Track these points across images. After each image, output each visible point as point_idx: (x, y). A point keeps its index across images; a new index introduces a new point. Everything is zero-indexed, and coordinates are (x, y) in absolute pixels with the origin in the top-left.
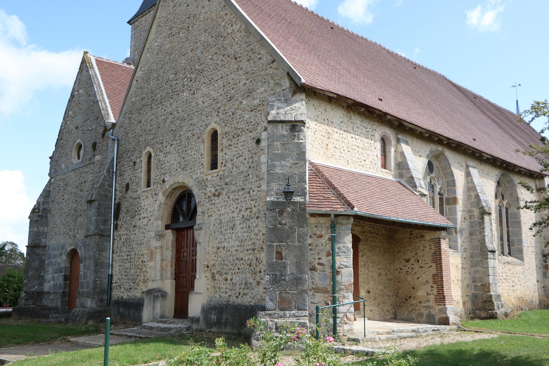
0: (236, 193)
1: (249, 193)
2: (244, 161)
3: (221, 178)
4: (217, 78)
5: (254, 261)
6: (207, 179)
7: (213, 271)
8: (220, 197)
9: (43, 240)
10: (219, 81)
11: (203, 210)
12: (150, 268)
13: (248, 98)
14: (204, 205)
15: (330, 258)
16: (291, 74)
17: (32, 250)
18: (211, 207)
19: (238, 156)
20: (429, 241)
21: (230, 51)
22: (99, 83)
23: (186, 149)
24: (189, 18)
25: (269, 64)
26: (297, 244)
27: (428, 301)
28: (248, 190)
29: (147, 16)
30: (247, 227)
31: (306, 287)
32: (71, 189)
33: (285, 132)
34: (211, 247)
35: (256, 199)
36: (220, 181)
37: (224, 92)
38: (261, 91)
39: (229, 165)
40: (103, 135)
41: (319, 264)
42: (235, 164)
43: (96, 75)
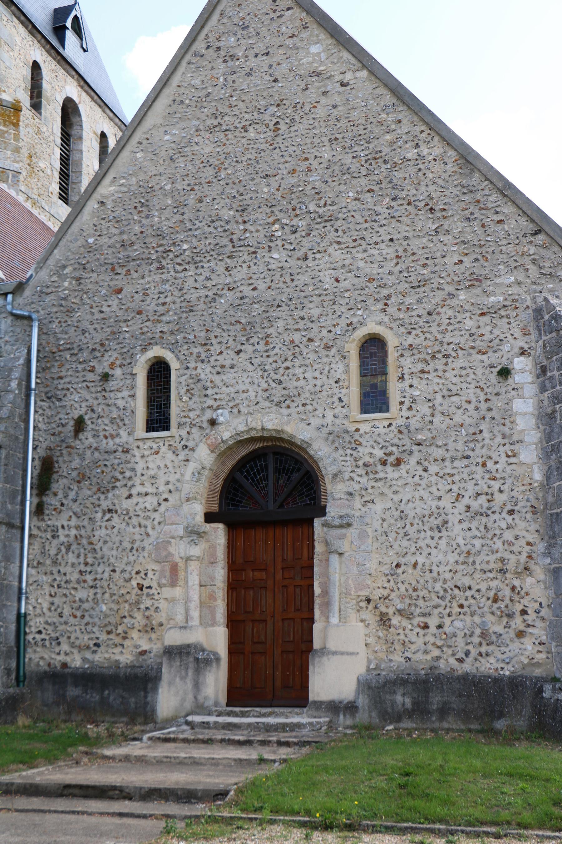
0: (448, 463)
1: (484, 465)
2: (465, 405)
4: (375, 239)
5: (507, 592)
6: (357, 430)
7: (383, 609)
8: (402, 466)
11: (351, 490)
12: (171, 601)
14: (351, 479)
18: (372, 483)
19: (446, 393)
24: (278, 105)
25: (525, 235)
28: (480, 460)
30: (482, 528)
35: (504, 478)
36: (401, 436)
37: (398, 268)
38: (507, 282)
42: (439, 408)
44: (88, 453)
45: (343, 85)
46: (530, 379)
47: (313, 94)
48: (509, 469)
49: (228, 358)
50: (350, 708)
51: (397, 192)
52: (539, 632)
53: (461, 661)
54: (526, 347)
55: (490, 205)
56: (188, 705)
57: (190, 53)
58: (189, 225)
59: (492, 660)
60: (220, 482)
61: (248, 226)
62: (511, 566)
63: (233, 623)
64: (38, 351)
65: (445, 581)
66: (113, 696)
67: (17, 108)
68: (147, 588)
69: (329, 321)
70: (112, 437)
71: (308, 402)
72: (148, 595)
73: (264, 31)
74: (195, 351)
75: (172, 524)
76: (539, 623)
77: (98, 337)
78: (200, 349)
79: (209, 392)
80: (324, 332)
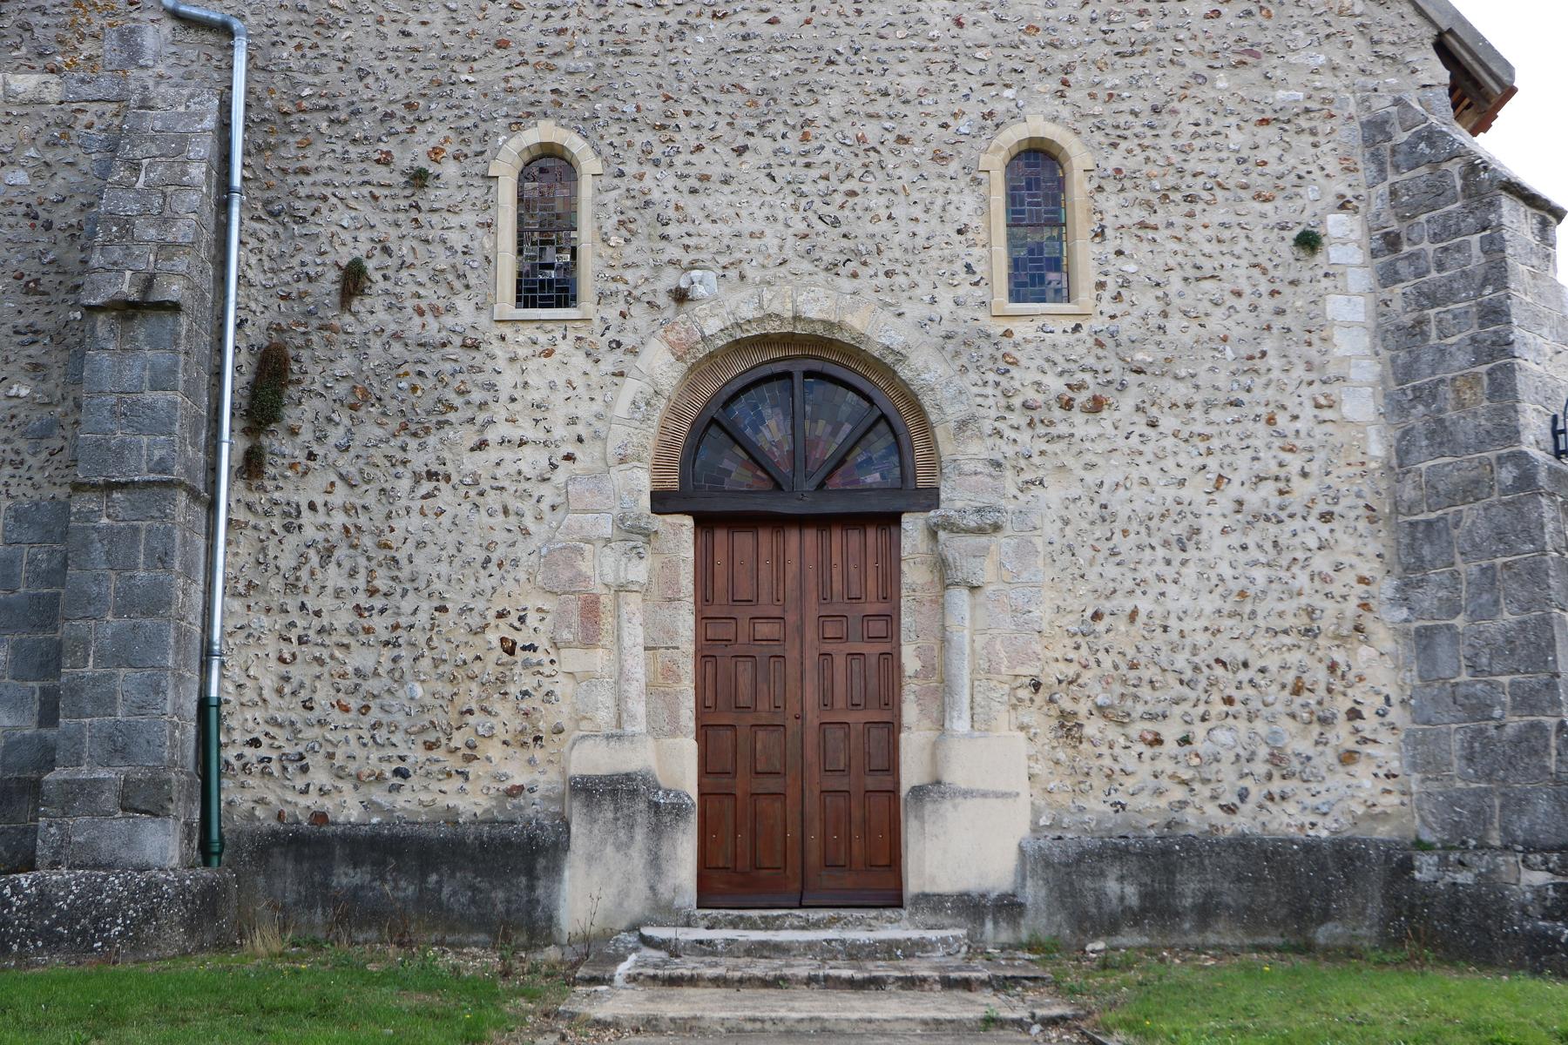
0: (1197, 412)
1: (1271, 421)
2: (1231, 300)
5: (1321, 675)
6: (1008, 334)
7: (1068, 705)
11: (998, 457)
13: (1241, 71)
18: (1042, 445)
38: (1312, 63)
42: (1176, 301)
44: (376, 344)
48: (1319, 431)
49: (715, 161)
50: (1008, 907)
52: (1387, 752)
53: (1230, 809)
54: (1349, 194)
59: (1291, 807)
62: (1326, 623)
65: (1195, 650)
66: (450, 888)
68: (524, 648)
69: (943, 105)
71: (899, 268)
72: (526, 664)
74: (639, 139)
75: (585, 511)
76: (1384, 736)
79: (672, 230)
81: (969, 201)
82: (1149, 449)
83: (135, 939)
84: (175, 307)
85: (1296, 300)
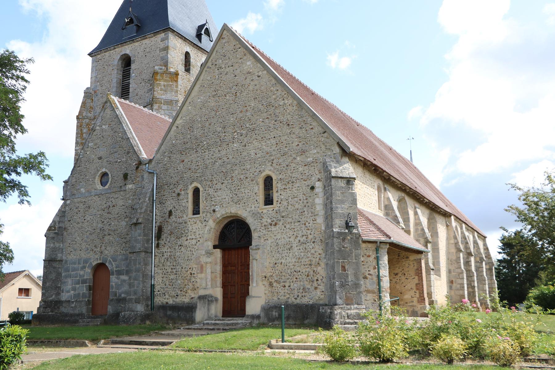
0: (293, 224)
1: (305, 224)
2: (299, 201)
3: (277, 212)
4: (269, 137)
5: (312, 273)
6: (262, 212)
7: (271, 280)
9: (59, 255)
10: (271, 140)
12: (201, 279)
14: (260, 231)
15: (376, 270)
16: (340, 143)
17: (49, 263)
18: (267, 233)
19: (293, 197)
20: (413, 261)
21: (281, 118)
22: (126, 122)
23: (239, 187)
25: (320, 134)
26: (354, 261)
27: (413, 302)
28: (304, 222)
29: (112, 52)
31: (362, 290)
32: (95, 211)
33: (343, 185)
34: (268, 262)
37: (277, 148)
39: (285, 203)
40: (137, 168)
41: (369, 274)
42: (290, 203)
43: (122, 115)
44: (173, 224)
45: (258, 77)
46: (321, 191)
47: (248, 81)
48: (313, 225)
49: (219, 186)
50: (258, 317)
51: (277, 118)
52: (322, 287)
53: (296, 299)
54: (320, 178)
55: (308, 122)
56: (206, 317)
57: (206, 67)
58: (206, 134)
59: (306, 298)
60: (219, 233)
61: (226, 134)
62: (313, 263)
63: (225, 286)
64: (156, 186)
65: (291, 269)
66: (182, 314)
67: (177, 74)
69: (252, 170)
70: (181, 217)
73: (231, 57)
74: (208, 183)
76: (322, 284)
77: (176, 179)
78: (210, 183)
79: (213, 199)
80: (251, 174)
81: (257, 188)
82: (284, 232)
83: (134, 322)
84: (141, 223)
85: (310, 200)
